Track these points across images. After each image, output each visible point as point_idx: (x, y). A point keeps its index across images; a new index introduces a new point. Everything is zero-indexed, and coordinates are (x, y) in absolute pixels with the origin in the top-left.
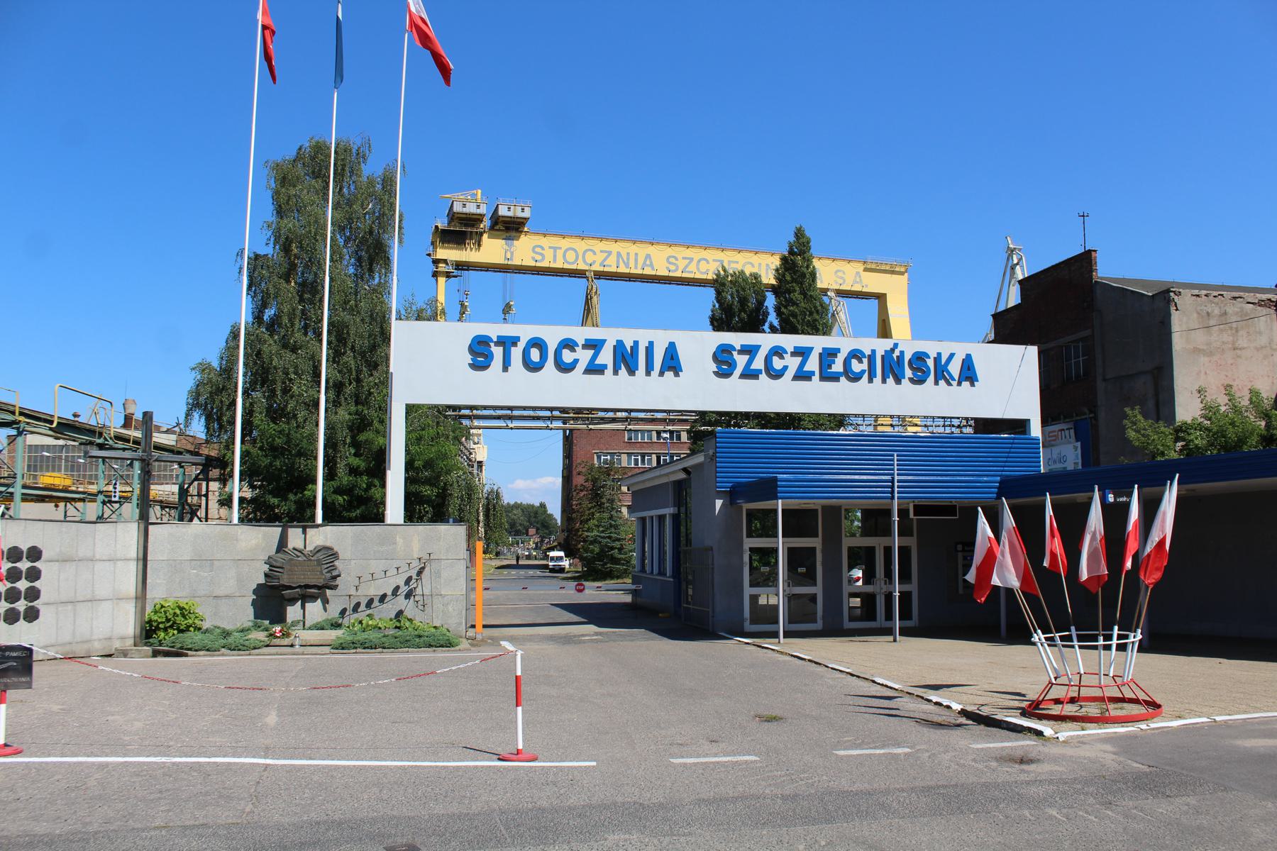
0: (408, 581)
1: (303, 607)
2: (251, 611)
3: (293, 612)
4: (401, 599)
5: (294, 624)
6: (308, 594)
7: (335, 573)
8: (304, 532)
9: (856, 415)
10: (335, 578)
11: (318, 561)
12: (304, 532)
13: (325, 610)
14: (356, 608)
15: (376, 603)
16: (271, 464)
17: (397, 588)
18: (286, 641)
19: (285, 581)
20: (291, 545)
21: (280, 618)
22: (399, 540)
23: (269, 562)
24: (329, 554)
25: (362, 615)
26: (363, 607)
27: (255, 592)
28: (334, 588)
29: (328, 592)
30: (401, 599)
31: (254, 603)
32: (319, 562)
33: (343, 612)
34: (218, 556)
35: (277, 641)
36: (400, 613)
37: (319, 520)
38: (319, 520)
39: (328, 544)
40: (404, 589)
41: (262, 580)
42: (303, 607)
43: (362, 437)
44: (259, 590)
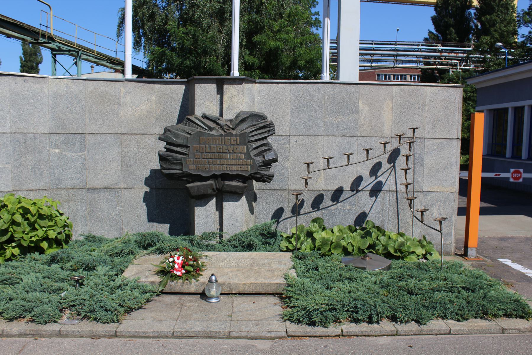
0: (375, 170)
1: (219, 208)
2: (143, 209)
3: (204, 217)
4: (364, 197)
5: (206, 236)
6: (227, 188)
7: (269, 156)
8: (220, 91)
9: (477, 76)
10: (268, 164)
11: (243, 136)
12: (220, 91)
13: (252, 210)
14: (296, 210)
15: (327, 201)
16: (182, 63)
17: (359, 179)
18: (194, 285)
19: (191, 168)
20: (199, 111)
21: (183, 226)
22: (363, 108)
23: (166, 137)
24: (259, 126)
25: (305, 220)
26: (307, 207)
27: (148, 181)
28: (268, 179)
29: (256, 185)
30: (364, 197)
31: (147, 198)
32: (244, 139)
33: (278, 214)
34: (92, 128)
35: (177, 285)
36: (361, 218)
37: (235, 72)
38: (235, 72)
39: (256, 109)
40: (368, 182)
41: (156, 165)
42: (219, 208)
43: (257, 38)
44: (154, 179)
